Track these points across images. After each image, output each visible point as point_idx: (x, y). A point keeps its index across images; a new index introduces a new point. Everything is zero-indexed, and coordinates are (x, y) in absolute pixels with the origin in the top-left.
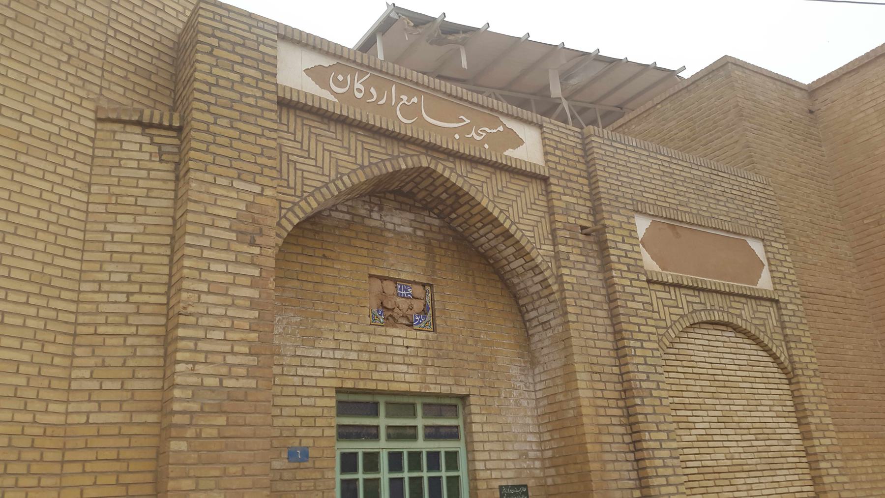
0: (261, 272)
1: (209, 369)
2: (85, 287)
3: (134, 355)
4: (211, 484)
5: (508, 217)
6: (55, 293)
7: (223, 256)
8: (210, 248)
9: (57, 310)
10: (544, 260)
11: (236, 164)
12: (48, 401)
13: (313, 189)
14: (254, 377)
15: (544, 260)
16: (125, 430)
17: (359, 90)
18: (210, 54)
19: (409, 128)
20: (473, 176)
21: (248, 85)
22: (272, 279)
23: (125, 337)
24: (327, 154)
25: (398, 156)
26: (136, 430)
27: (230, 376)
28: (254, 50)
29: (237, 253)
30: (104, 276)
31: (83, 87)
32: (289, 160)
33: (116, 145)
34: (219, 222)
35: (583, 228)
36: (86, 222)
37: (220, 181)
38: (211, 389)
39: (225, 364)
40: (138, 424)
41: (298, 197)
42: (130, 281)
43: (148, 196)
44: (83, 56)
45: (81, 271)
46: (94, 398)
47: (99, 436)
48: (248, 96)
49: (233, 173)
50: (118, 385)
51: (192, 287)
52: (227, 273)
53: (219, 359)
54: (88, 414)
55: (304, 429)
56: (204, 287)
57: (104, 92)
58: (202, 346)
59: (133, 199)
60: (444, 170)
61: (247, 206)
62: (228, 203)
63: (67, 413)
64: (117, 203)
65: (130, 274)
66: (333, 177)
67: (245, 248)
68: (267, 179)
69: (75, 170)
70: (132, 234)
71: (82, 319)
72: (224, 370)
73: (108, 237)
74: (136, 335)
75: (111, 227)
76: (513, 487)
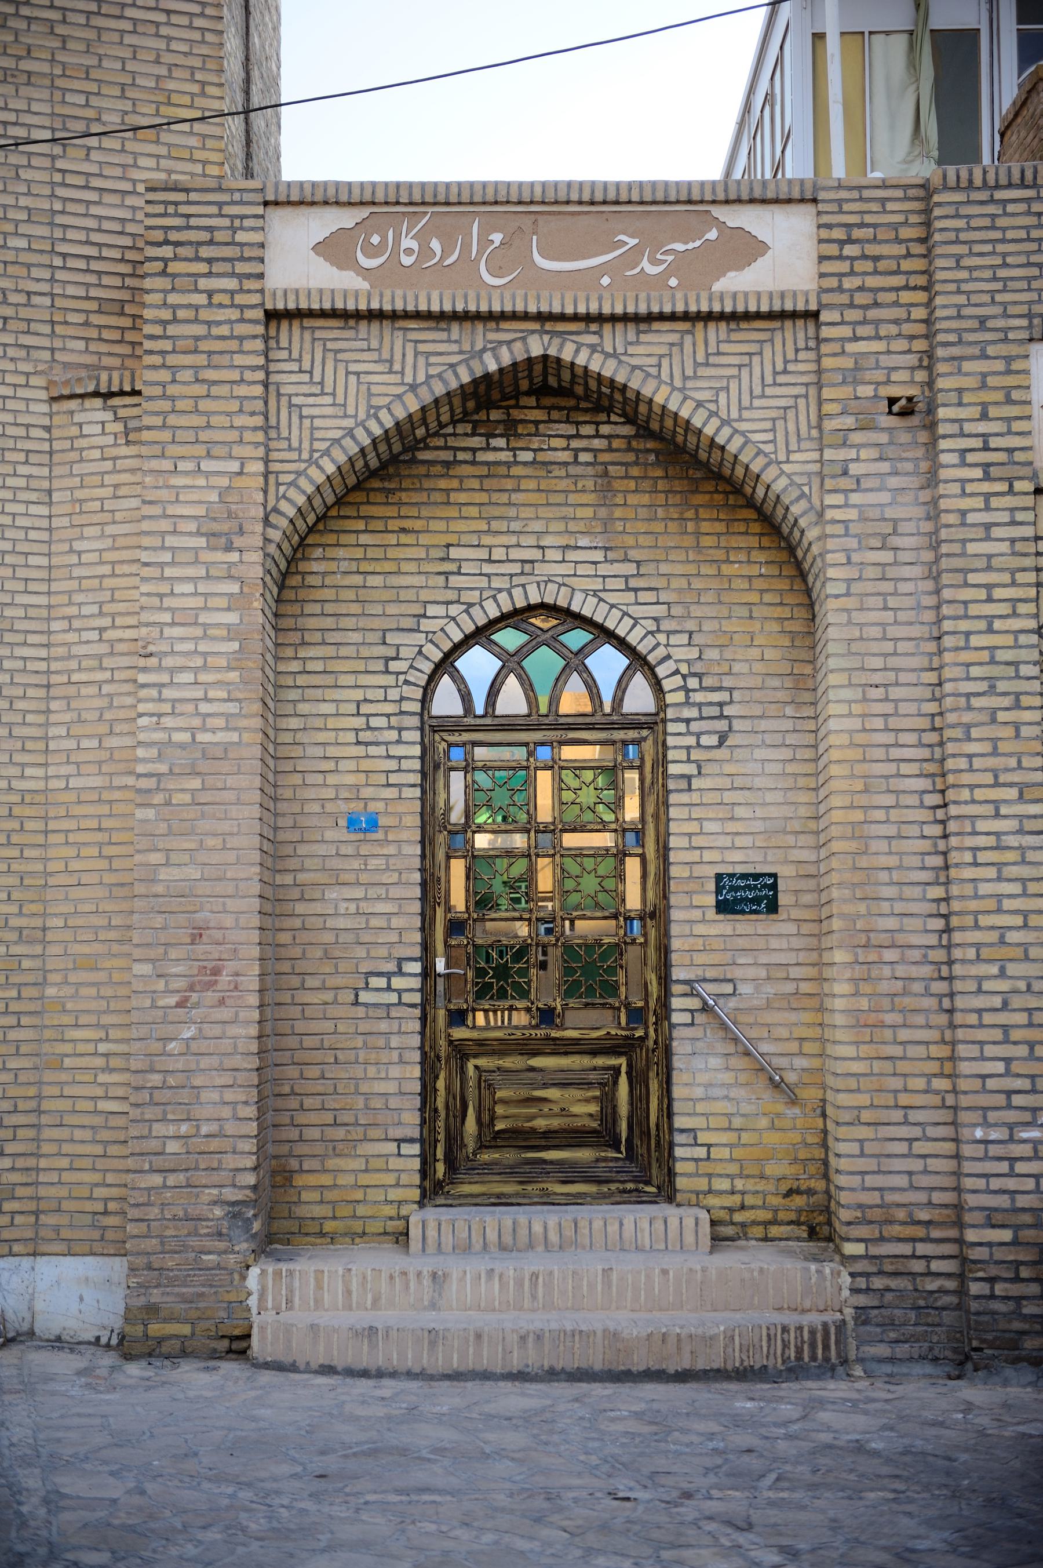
1: (180, 722)
2: (55, 626)
3: (111, 706)
4: (185, 858)
6: (19, 638)
7: (190, 572)
8: (173, 563)
9: (24, 659)
10: (792, 483)
11: (203, 436)
12: (23, 765)
14: (235, 729)
15: (792, 483)
16: (106, 796)
17: (409, 251)
18: (164, 273)
21: (221, 305)
23: (100, 684)
24: (353, 379)
25: (484, 350)
26: (117, 795)
27: (204, 729)
28: (227, 244)
29: (208, 565)
30: (73, 610)
31: (27, 359)
33: (74, 431)
34: (183, 526)
35: (892, 401)
36: (49, 543)
37: (182, 466)
38: (182, 746)
39: (198, 714)
40: (119, 788)
42: (101, 614)
43: (115, 497)
44: (24, 313)
45: (49, 607)
46: (72, 759)
47: (79, 802)
48: (219, 323)
49: (200, 450)
50: (95, 743)
51: (152, 619)
52: (196, 594)
53: (190, 708)
54: (68, 777)
55: (371, 789)
56: (167, 618)
57: (58, 356)
58: (167, 693)
59: (98, 503)
60: (577, 351)
62: (195, 497)
63: (47, 778)
64: (81, 512)
65: (101, 604)
66: (362, 415)
68: (250, 447)
69: (29, 477)
70: (100, 551)
71: (55, 666)
72: (196, 722)
73: (74, 559)
74: (112, 681)
75: (78, 546)
76: (744, 876)
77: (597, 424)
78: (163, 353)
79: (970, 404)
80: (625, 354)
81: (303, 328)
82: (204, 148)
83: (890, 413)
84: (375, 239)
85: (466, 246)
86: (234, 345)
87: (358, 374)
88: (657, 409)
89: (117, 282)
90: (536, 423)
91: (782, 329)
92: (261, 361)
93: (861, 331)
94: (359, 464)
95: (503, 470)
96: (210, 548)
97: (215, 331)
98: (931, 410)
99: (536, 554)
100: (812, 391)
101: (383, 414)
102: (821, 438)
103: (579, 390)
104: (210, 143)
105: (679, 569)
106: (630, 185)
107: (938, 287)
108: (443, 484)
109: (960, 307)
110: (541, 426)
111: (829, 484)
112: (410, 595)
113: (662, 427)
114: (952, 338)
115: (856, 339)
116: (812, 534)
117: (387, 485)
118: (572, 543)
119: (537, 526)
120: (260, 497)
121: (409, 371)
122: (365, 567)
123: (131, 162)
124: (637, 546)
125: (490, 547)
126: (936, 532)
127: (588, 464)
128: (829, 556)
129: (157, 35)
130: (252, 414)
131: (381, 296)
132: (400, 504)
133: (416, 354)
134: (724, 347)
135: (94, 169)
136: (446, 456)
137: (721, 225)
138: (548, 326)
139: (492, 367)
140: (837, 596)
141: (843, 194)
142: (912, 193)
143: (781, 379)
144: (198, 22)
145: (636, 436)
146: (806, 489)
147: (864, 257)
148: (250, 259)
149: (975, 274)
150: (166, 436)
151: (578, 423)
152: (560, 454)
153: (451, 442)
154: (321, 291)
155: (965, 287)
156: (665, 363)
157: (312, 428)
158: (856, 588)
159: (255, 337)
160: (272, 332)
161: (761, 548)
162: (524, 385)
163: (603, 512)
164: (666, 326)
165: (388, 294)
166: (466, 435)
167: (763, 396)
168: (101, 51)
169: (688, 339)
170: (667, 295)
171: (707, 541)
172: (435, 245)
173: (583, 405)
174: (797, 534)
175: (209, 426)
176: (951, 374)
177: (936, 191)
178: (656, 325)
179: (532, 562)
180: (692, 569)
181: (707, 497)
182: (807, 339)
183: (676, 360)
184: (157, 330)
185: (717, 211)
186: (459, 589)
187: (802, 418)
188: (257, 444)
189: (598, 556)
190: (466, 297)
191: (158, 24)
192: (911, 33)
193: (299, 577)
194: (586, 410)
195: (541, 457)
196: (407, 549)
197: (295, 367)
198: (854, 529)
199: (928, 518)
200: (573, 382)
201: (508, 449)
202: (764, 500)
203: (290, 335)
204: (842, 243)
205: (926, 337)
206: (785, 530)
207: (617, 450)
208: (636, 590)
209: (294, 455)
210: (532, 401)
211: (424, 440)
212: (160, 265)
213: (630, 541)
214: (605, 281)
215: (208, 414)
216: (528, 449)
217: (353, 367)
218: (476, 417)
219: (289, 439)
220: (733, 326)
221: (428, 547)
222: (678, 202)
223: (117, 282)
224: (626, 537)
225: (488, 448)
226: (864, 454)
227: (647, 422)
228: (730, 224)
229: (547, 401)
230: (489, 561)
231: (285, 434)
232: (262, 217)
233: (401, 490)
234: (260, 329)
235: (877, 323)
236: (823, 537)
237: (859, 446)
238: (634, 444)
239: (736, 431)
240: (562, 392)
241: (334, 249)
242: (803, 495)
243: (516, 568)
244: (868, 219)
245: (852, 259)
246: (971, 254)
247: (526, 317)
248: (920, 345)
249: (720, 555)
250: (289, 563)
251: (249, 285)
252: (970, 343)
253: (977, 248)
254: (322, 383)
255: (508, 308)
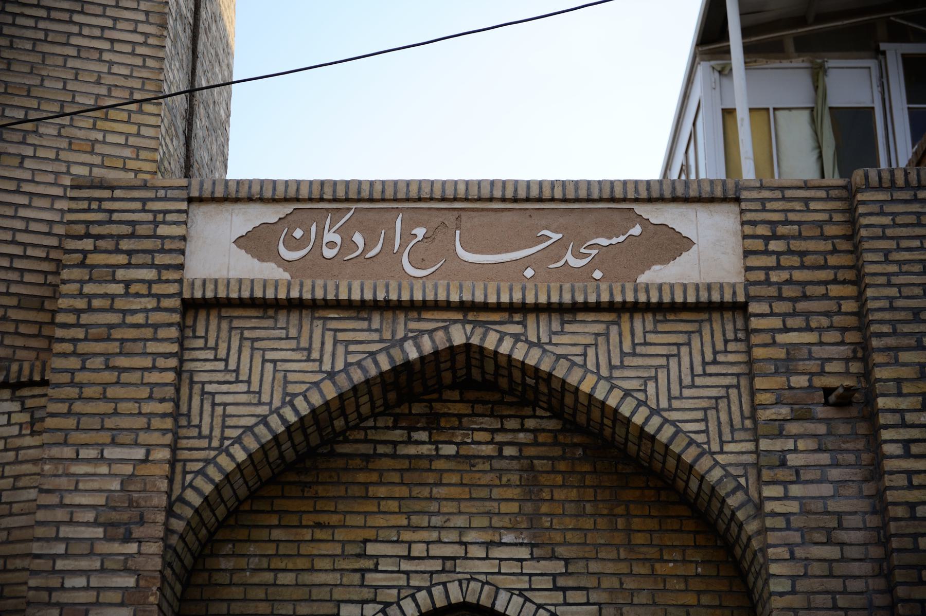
0: (137, 581)
5: (641, 403)
7: (84, 564)
10: (727, 474)
13: (240, 431)
15: (727, 474)
17: (331, 245)
18: (82, 264)
19: (418, 286)
20: (565, 339)
21: (138, 295)
22: (154, 589)
24: (269, 367)
25: (405, 338)
29: (103, 557)
32: (203, 393)
35: (828, 391)
37: (84, 453)
41: (214, 449)
48: (134, 312)
49: (105, 437)
61: (122, 483)
62: (96, 485)
66: (277, 403)
67: (116, 548)
68: (157, 434)
77: (523, 418)
78: (74, 341)
79: (910, 395)
80: (550, 343)
81: (220, 318)
82: (137, 158)
83: (826, 404)
84: (298, 233)
85: (389, 240)
86: (148, 333)
87: (274, 362)
88: (583, 400)
89: (40, 279)
90: (460, 416)
91: (710, 320)
92: (175, 348)
93: (790, 323)
94: (274, 454)
95: (424, 464)
96: (107, 539)
97: (130, 319)
98: (870, 398)
99: (458, 551)
100: (744, 382)
101: (300, 403)
102: (755, 429)
103: (503, 383)
104: (143, 154)
105: (610, 568)
106: (553, 184)
107: (868, 280)
108: (361, 477)
109: (891, 299)
110: (465, 420)
111: (766, 475)
112: (324, 593)
113: (589, 420)
114: (886, 329)
115: (786, 330)
116: (752, 527)
117: (303, 478)
118: (496, 539)
119: (460, 521)
120: (164, 485)
121: (327, 358)
122: (277, 563)
123: (64, 169)
124: (565, 543)
125: (410, 543)
126: (885, 526)
127: (512, 458)
128: (770, 550)
129: (100, 60)
130: (162, 400)
131: (301, 285)
132: (316, 498)
133: (336, 342)
134: (651, 338)
135: (27, 175)
136: (364, 449)
137: (645, 222)
138: (470, 317)
139: (413, 355)
140: (781, 594)
141: (766, 194)
142: (833, 193)
143: (711, 369)
144: (140, 50)
145: (563, 430)
146: (742, 481)
147: (790, 252)
148: (170, 251)
149: (905, 268)
150: (71, 423)
151: (502, 417)
152: (484, 447)
153: (372, 435)
154: (240, 281)
155: (895, 280)
156: (591, 352)
157: (225, 416)
158: (802, 585)
159: (170, 325)
160: (189, 322)
161: (696, 546)
162: (447, 377)
163: (528, 507)
164: (591, 317)
165: (308, 284)
166: (387, 428)
167: (693, 386)
168: (44, 73)
169: (614, 330)
170: (591, 286)
171: (639, 539)
172: (358, 238)
173: (508, 399)
174: (734, 528)
175: (116, 413)
176: (887, 364)
177: (859, 190)
178: (580, 316)
179: (454, 559)
180: (623, 568)
181: (638, 493)
182: (736, 330)
183: (602, 349)
184: (71, 319)
185: (640, 209)
186: (376, 588)
187: (735, 408)
188: (164, 431)
189: (524, 553)
190: (387, 286)
191: (101, 51)
192: (812, 109)
193: (206, 575)
194: (511, 404)
195: (464, 451)
196: (322, 545)
197: (210, 355)
198: (796, 522)
199: (874, 512)
200: (496, 374)
201: (430, 443)
202: (698, 494)
203: (209, 327)
204: (767, 239)
205: (858, 329)
206: (722, 526)
207: (543, 444)
208: (564, 590)
209: (204, 443)
210: (456, 395)
211: (343, 432)
212: (79, 256)
213: (558, 538)
214: (529, 273)
215: (116, 401)
216: (451, 443)
217: (270, 355)
218: (398, 410)
219: (199, 427)
220: (659, 317)
221: (344, 543)
222: (601, 200)
223: (40, 279)
224: (553, 534)
225: (409, 441)
226: (801, 445)
227: (574, 416)
228: (653, 221)
229: (471, 395)
230: (409, 558)
231: (196, 421)
232: (186, 212)
233: (317, 483)
234: (176, 318)
235: (807, 315)
236: (763, 531)
237: (796, 437)
238: (561, 438)
239: (666, 421)
240: (489, 385)
241: (255, 243)
242: (739, 487)
243: (436, 566)
244: (792, 217)
245: (778, 254)
246: (899, 249)
247: (448, 306)
248: (852, 337)
249: (652, 553)
250: (195, 559)
251: (166, 275)
252: (905, 335)
253: (904, 244)
254: (237, 371)
255: (430, 297)
